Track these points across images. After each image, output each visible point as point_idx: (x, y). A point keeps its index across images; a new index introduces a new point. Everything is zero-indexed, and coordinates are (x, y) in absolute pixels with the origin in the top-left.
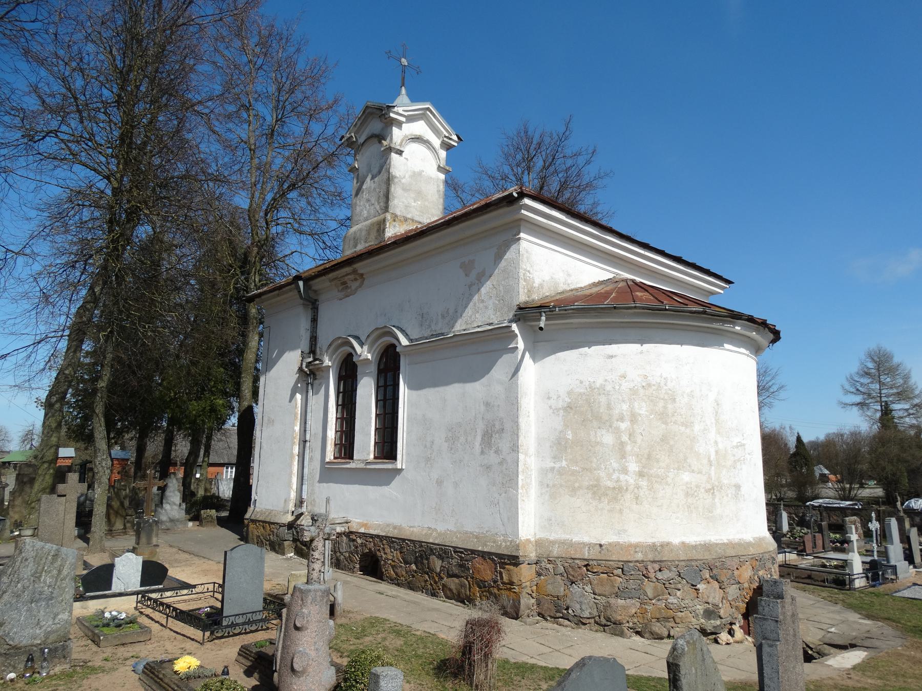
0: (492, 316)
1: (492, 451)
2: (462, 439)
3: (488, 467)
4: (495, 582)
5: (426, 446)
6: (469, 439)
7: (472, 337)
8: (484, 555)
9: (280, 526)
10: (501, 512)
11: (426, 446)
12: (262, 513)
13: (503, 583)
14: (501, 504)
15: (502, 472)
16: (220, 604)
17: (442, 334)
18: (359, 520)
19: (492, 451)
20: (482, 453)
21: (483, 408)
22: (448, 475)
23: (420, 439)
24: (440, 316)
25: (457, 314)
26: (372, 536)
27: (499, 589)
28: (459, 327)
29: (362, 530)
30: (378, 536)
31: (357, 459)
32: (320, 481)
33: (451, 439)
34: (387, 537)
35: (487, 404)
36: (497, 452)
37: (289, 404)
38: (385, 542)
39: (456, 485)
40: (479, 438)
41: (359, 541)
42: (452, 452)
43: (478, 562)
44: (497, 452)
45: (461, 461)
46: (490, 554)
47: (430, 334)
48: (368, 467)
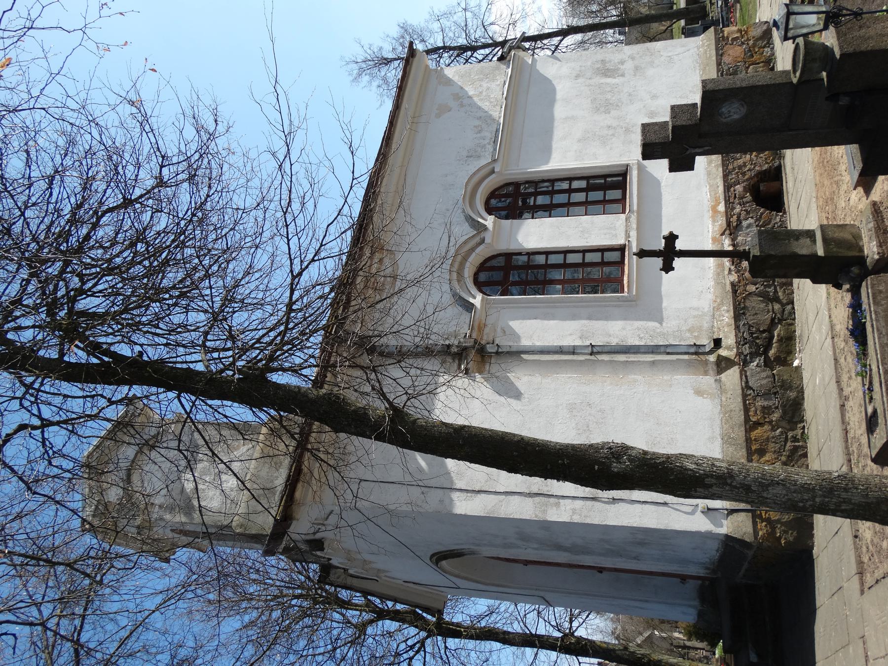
0: (499, 83)
1: (622, 67)
2: (609, 96)
3: (637, 68)
4: (743, 43)
5: (613, 135)
6: (609, 89)
7: (511, 91)
8: (720, 56)
9: (748, 387)
10: (677, 53)
11: (613, 135)
12: (727, 440)
13: (742, 37)
14: (670, 54)
15: (641, 57)
16: (581, 661)
17: (497, 131)
18: (710, 226)
19: (622, 67)
20: (623, 75)
21: (580, 80)
22: (644, 107)
23: (604, 142)
24: (479, 135)
25: (488, 119)
26: (728, 187)
27: (748, 40)
28: (498, 114)
29: (721, 208)
30: (725, 176)
31: (623, 235)
32: (660, 321)
33: (607, 108)
34: (723, 164)
35: (577, 77)
36: (622, 62)
37: (525, 400)
38: (730, 167)
39: (654, 97)
40: (609, 80)
41: (738, 209)
42: (620, 104)
43: (726, 59)
44: (622, 62)
45: (630, 95)
46: (717, 49)
47: (492, 143)
48: (635, 208)
